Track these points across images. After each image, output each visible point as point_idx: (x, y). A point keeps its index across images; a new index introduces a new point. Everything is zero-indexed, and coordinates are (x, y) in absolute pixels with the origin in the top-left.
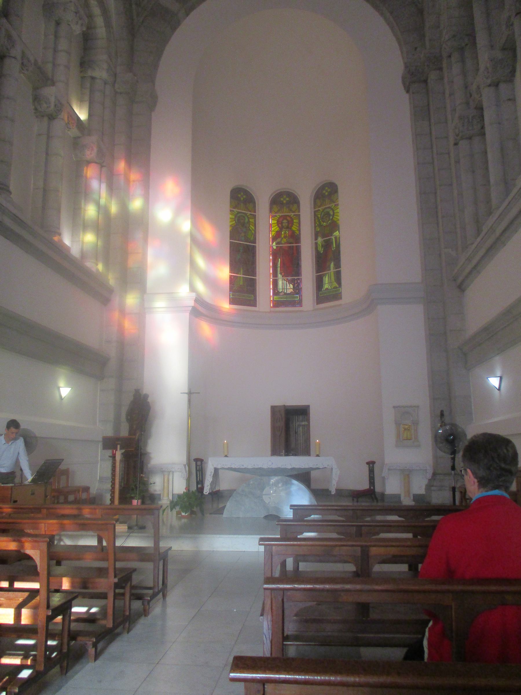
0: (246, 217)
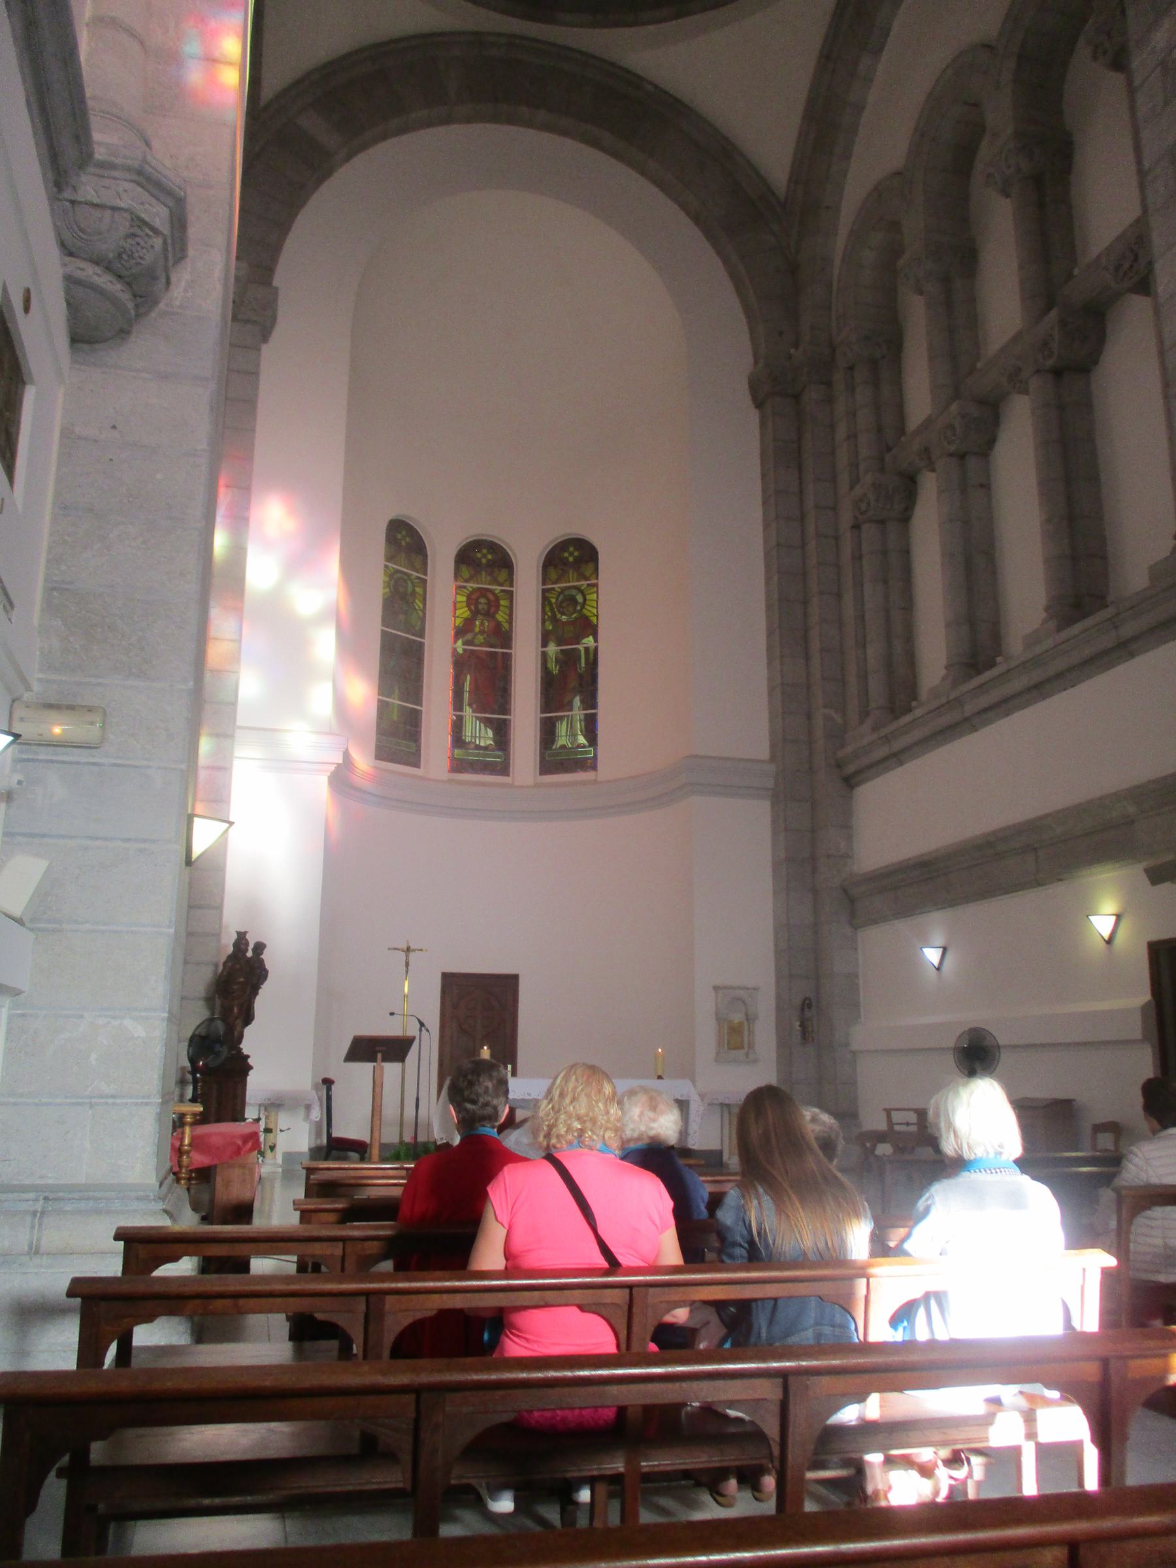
0: (409, 582)
